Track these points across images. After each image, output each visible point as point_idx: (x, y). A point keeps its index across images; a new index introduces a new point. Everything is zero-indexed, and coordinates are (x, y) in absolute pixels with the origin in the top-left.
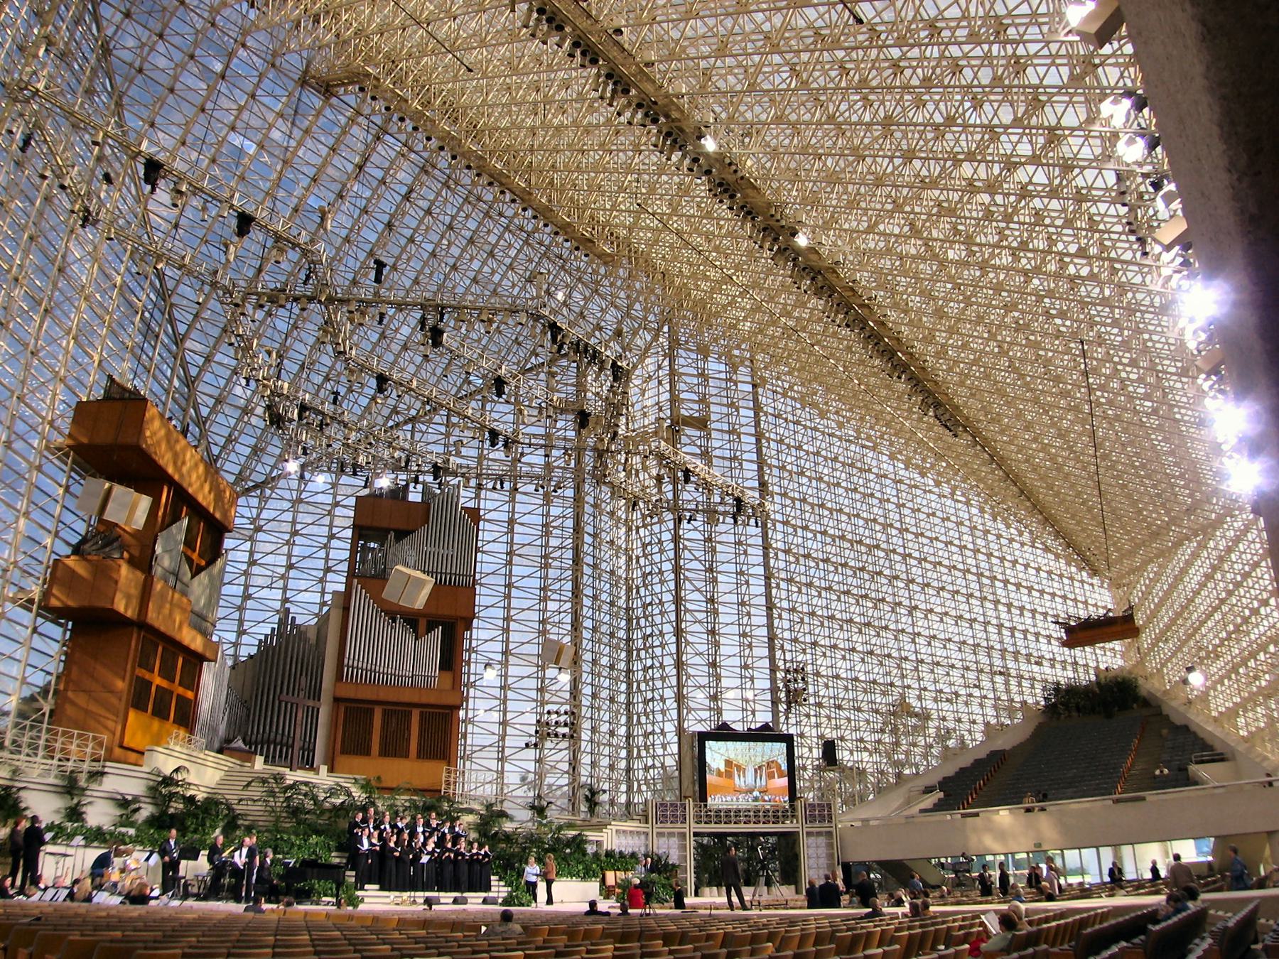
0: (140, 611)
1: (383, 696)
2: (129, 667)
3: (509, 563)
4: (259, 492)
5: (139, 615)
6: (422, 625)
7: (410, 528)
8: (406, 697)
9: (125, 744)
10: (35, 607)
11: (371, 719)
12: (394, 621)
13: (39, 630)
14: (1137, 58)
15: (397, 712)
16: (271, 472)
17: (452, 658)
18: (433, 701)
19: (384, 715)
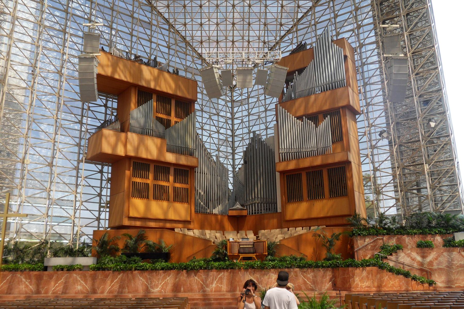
6: (320, 116)
7: (305, 66)
15: (314, 172)
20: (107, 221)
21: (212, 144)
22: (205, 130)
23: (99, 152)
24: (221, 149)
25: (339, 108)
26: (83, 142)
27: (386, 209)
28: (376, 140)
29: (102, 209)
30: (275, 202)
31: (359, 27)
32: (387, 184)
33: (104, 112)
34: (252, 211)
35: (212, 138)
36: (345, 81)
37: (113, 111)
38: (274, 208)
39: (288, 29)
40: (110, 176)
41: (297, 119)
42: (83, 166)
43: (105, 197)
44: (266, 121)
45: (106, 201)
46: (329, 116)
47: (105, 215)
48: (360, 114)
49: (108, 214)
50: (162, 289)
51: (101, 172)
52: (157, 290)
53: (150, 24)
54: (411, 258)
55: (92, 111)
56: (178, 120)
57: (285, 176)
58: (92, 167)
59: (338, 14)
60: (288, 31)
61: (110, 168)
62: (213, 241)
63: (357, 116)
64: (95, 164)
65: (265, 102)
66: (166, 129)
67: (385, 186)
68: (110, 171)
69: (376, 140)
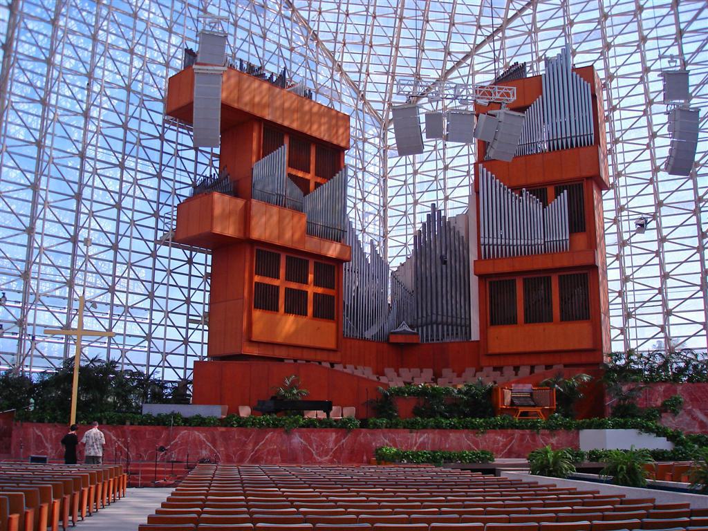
0: (581, 199)
1: (518, 267)
2: (247, 275)
3: (29, 262)
4: (500, 35)
5: (245, 233)
6: (550, 191)
7: (527, 104)
8: (539, 264)
9: (253, 339)
10: (170, 242)
11: (513, 291)
12: (521, 195)
13: (659, 329)
14: (220, 157)
15: (537, 279)
16: (507, 14)
17: (582, 220)
18: (566, 264)
19: (525, 284)
20: (206, 347)
21: (178, 172)
22: (167, 141)
23: (207, 230)
24: (164, 174)
25: (581, 179)
26: (164, 211)
27: (640, 342)
28: (629, 231)
29: (191, 325)
30: (468, 323)
31: (608, 46)
32: (645, 302)
33: (159, 149)
34: (427, 336)
35: (181, 158)
36: (593, 136)
37: (214, 159)
38: (466, 333)
39: (489, 34)
40: (209, 270)
41: (512, 191)
42: (163, 250)
43: (125, 294)
44: (445, 186)
45: (204, 312)
46: (565, 191)
47: (199, 336)
48: (609, 189)
49: (206, 334)
50: (334, 457)
51: (190, 262)
52: (326, 458)
53: (263, 7)
54: (692, 416)
55: (144, 147)
56: (319, 180)
57: (488, 283)
58: (178, 253)
59: (575, 21)
60: (488, 37)
61: (210, 257)
62: (401, 385)
63: (603, 192)
64: (184, 249)
65: (444, 154)
66: (305, 195)
67: (641, 306)
68: (209, 262)
69: (629, 231)
